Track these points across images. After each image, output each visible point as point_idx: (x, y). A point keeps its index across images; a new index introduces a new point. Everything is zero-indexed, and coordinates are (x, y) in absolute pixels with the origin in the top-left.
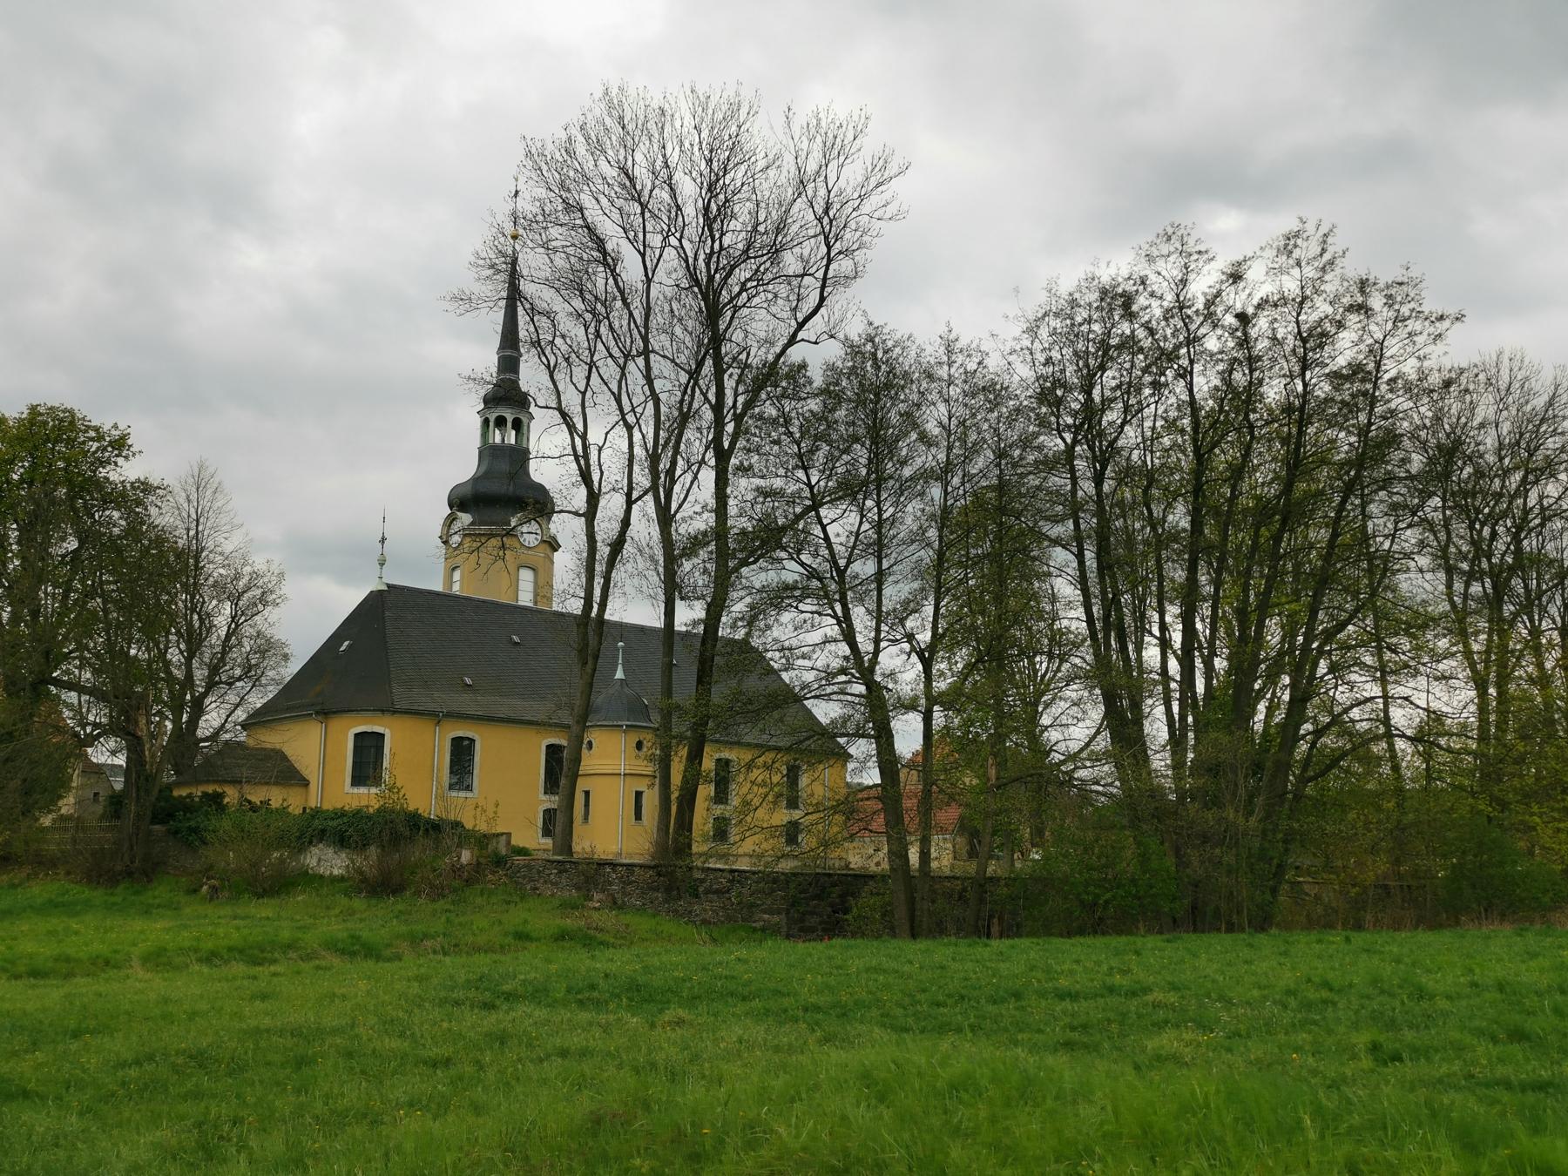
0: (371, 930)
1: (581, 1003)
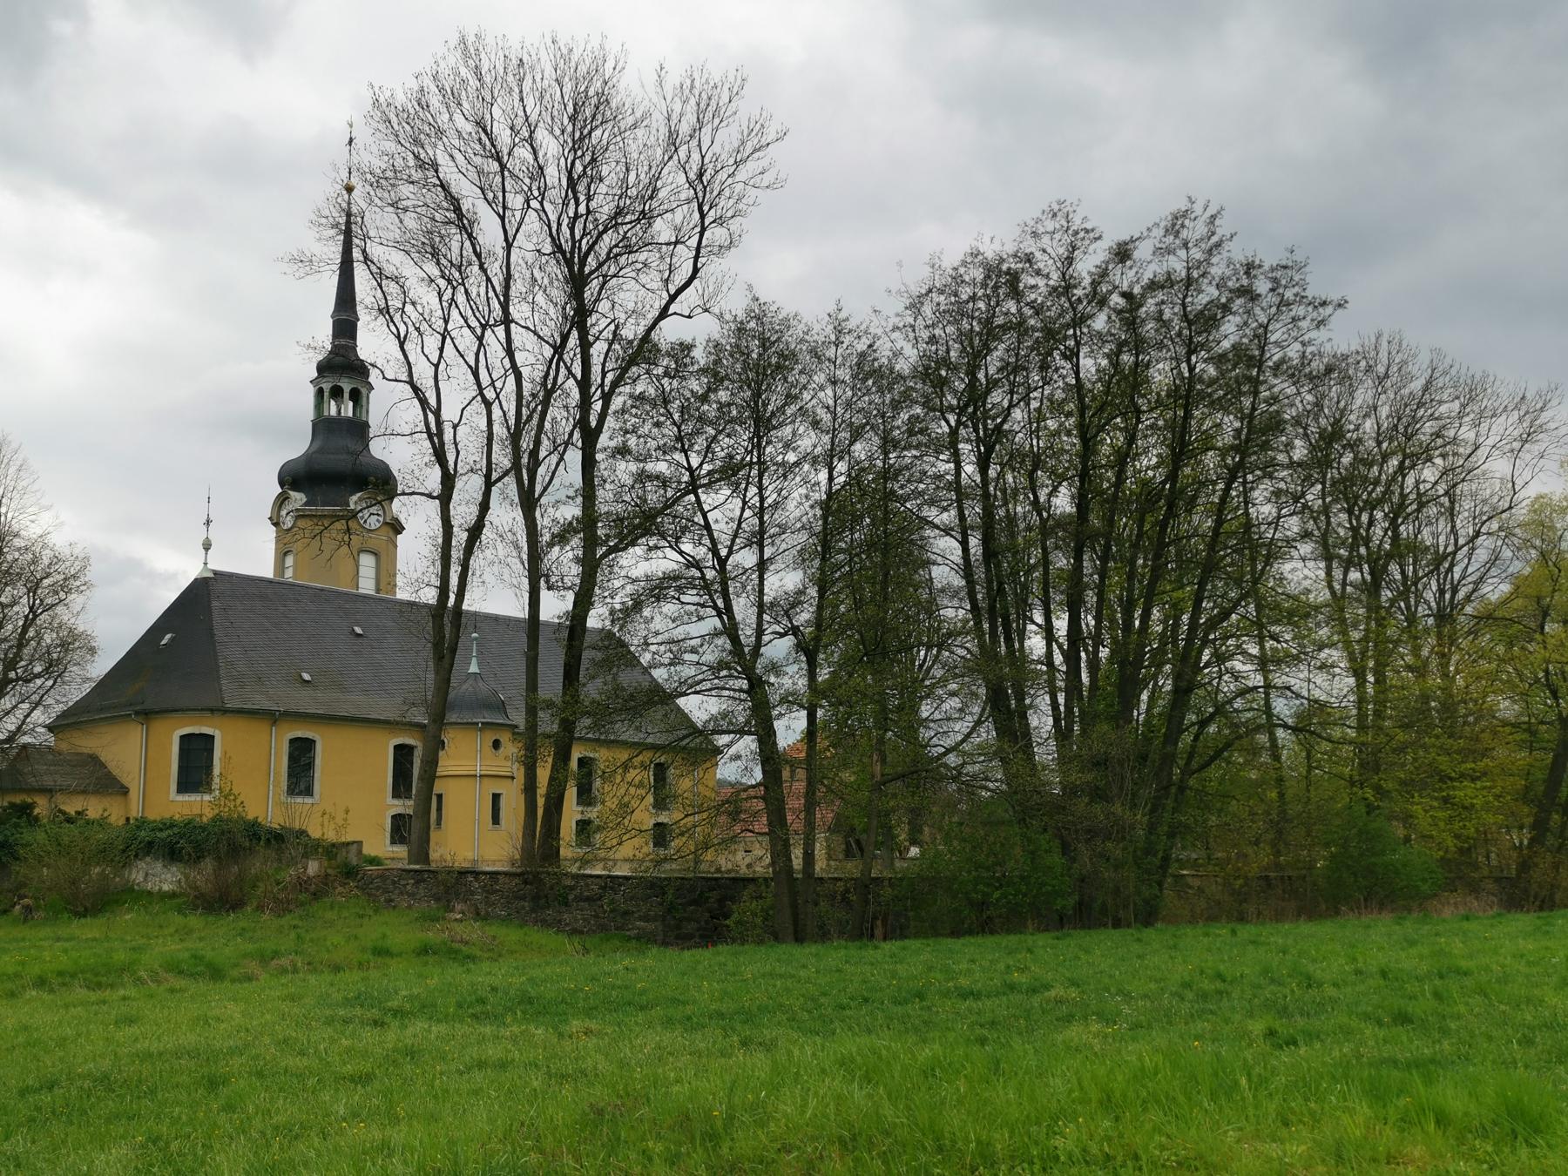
0: (213, 949)
1: (475, 1016)
